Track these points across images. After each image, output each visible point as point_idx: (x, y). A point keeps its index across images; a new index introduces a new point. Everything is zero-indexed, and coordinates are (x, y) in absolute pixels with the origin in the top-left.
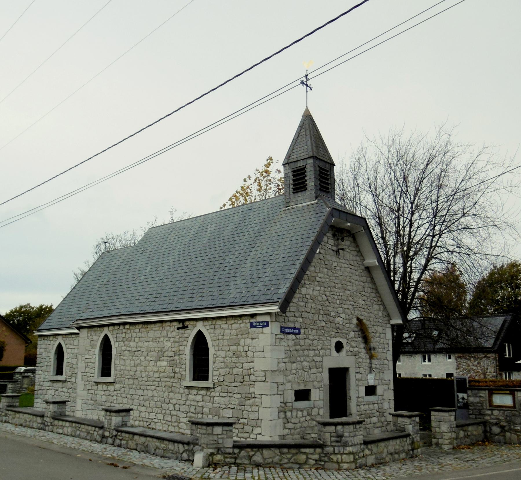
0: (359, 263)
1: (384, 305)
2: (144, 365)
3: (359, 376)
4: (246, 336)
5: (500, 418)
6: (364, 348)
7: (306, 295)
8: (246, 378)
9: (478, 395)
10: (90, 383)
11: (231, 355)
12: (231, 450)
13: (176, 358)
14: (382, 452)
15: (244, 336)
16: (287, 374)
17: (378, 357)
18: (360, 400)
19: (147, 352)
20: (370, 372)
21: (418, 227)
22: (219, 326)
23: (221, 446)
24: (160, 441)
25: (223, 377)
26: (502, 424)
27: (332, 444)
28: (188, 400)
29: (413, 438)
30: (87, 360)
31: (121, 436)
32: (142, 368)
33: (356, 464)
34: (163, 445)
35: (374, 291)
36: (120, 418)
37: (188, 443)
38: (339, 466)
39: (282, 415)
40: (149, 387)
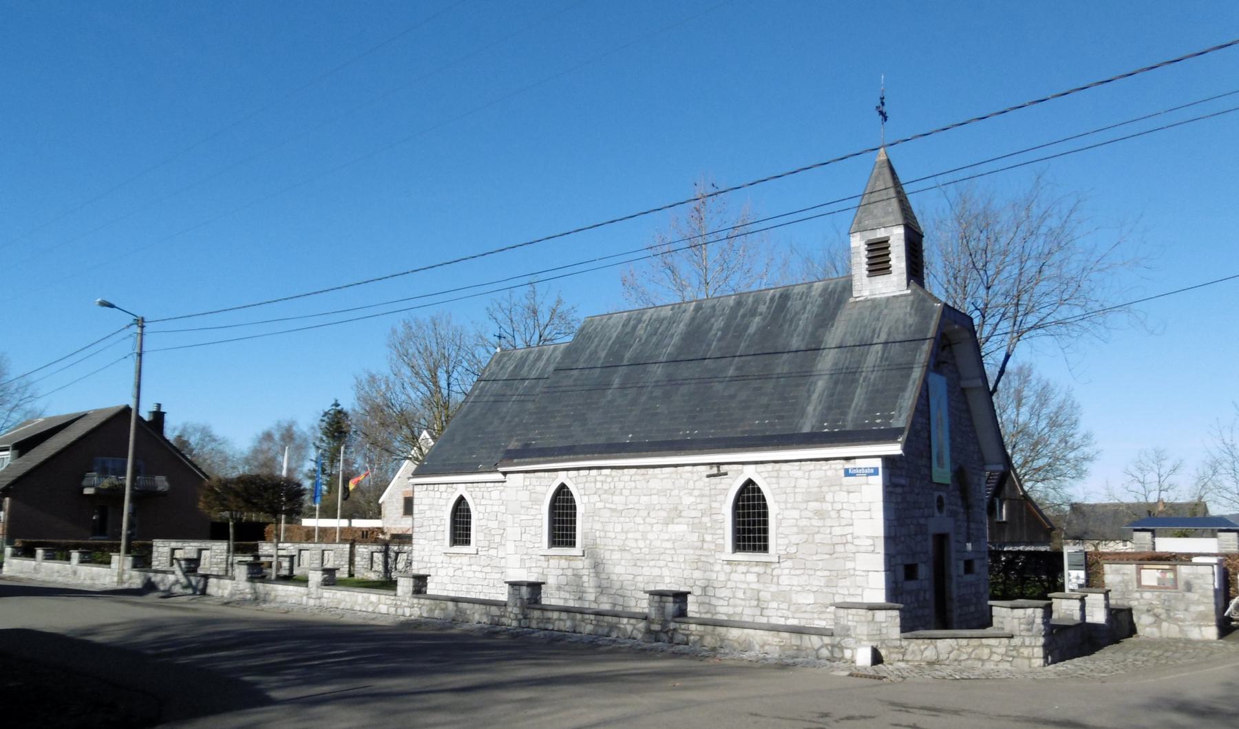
4: (837, 488)
8: (839, 548)
11: (811, 515)
13: (706, 519)
15: (833, 489)
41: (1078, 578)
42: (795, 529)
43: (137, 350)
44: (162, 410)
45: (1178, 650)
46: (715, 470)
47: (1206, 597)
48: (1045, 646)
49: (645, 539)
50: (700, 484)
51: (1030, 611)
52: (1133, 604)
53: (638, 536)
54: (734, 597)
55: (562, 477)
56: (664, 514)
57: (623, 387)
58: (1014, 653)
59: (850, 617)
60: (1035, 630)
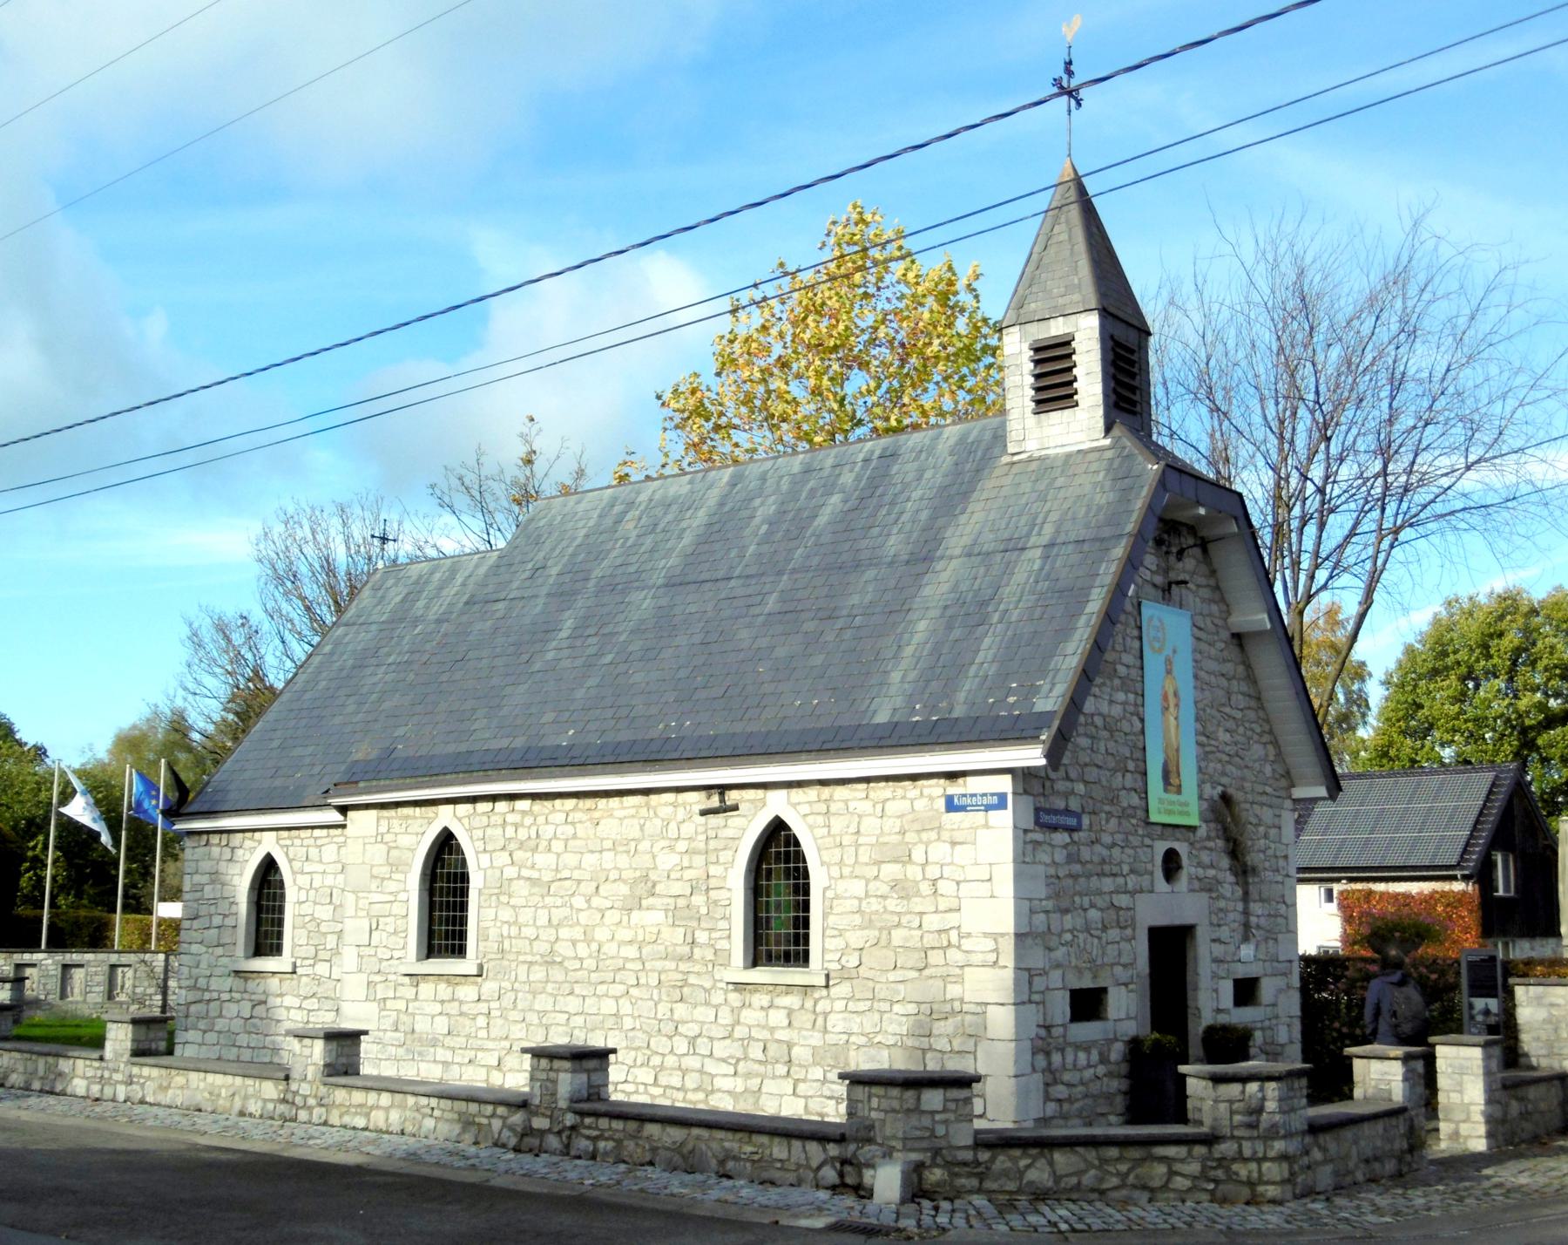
0: (1217, 621)
1: (1275, 743)
2: (582, 922)
3: (1218, 950)
4: (933, 835)
8: (935, 957)
9: (1547, 1001)
10: (391, 977)
11: (884, 889)
12: (968, 1155)
13: (699, 900)
14: (1347, 1156)
15: (924, 836)
16: (1052, 944)
17: (1264, 896)
19: (594, 884)
20: (1246, 939)
22: (842, 805)
23: (943, 1143)
24: (739, 1135)
25: (857, 954)
27: (1236, 1133)
28: (738, 1022)
29: (1412, 1120)
30: (376, 909)
31: (597, 1128)
32: (577, 933)
33: (1295, 1185)
34: (749, 1149)
35: (1253, 703)
36: (584, 1077)
37: (841, 1139)
38: (1253, 1192)
39: (1041, 1061)
40: (601, 989)
41: (1487, 1012)
42: (857, 919)
46: (715, 801)
49: (588, 940)
50: (688, 829)
51: (1253, 1087)
53: (577, 933)
54: (746, 1058)
55: (445, 817)
56: (624, 889)
57: (578, 633)
58: (1220, 1174)
59: (875, 1102)
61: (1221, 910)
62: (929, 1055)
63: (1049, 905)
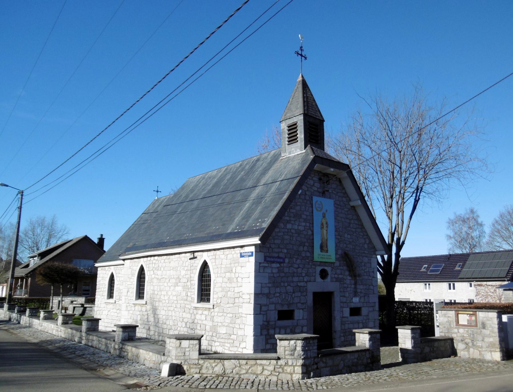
4: (237, 264)
5: (465, 335)
6: (349, 275)
7: (291, 229)
8: (237, 300)
9: (447, 316)
13: (189, 284)
18: (344, 319)
20: (355, 296)
21: (410, 174)
26: (466, 340)
39: (265, 332)
43: (19, 205)
44: (103, 237)
45: (477, 365)
47: (493, 332)
48: (303, 365)
51: (292, 342)
52: (454, 336)
55: (142, 261)
58: (280, 370)
60: (296, 354)
61: (345, 287)
62: (234, 329)
63: (270, 285)
